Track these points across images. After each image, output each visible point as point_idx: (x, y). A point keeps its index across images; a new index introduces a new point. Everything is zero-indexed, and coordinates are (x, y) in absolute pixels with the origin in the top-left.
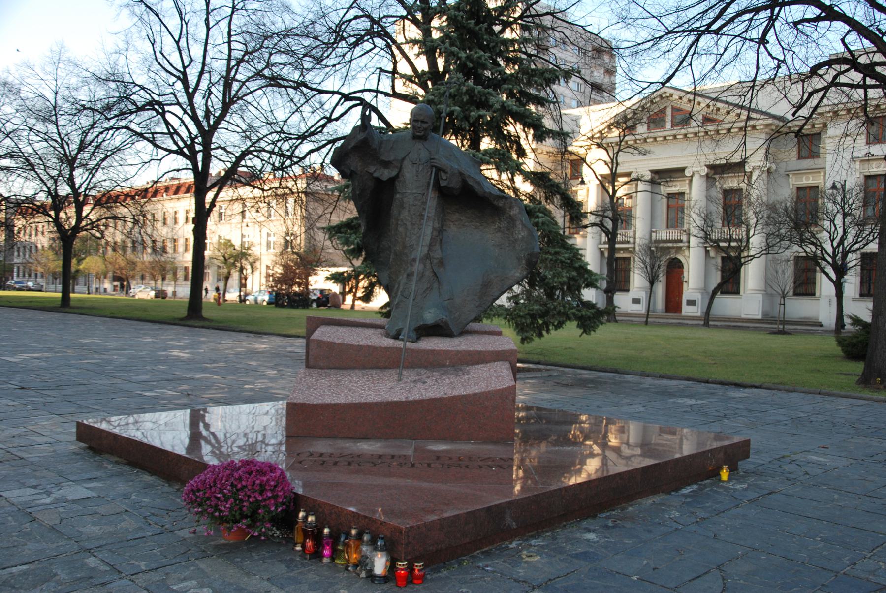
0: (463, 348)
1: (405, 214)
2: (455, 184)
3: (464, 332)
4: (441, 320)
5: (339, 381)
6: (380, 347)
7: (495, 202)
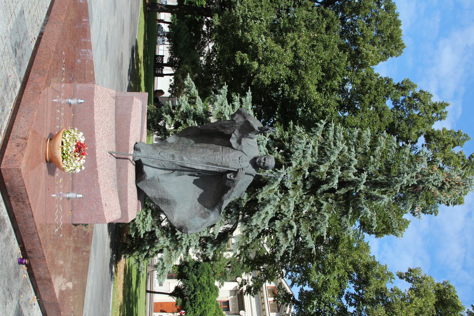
0: (129, 190)
1: (210, 152)
5: (108, 115)
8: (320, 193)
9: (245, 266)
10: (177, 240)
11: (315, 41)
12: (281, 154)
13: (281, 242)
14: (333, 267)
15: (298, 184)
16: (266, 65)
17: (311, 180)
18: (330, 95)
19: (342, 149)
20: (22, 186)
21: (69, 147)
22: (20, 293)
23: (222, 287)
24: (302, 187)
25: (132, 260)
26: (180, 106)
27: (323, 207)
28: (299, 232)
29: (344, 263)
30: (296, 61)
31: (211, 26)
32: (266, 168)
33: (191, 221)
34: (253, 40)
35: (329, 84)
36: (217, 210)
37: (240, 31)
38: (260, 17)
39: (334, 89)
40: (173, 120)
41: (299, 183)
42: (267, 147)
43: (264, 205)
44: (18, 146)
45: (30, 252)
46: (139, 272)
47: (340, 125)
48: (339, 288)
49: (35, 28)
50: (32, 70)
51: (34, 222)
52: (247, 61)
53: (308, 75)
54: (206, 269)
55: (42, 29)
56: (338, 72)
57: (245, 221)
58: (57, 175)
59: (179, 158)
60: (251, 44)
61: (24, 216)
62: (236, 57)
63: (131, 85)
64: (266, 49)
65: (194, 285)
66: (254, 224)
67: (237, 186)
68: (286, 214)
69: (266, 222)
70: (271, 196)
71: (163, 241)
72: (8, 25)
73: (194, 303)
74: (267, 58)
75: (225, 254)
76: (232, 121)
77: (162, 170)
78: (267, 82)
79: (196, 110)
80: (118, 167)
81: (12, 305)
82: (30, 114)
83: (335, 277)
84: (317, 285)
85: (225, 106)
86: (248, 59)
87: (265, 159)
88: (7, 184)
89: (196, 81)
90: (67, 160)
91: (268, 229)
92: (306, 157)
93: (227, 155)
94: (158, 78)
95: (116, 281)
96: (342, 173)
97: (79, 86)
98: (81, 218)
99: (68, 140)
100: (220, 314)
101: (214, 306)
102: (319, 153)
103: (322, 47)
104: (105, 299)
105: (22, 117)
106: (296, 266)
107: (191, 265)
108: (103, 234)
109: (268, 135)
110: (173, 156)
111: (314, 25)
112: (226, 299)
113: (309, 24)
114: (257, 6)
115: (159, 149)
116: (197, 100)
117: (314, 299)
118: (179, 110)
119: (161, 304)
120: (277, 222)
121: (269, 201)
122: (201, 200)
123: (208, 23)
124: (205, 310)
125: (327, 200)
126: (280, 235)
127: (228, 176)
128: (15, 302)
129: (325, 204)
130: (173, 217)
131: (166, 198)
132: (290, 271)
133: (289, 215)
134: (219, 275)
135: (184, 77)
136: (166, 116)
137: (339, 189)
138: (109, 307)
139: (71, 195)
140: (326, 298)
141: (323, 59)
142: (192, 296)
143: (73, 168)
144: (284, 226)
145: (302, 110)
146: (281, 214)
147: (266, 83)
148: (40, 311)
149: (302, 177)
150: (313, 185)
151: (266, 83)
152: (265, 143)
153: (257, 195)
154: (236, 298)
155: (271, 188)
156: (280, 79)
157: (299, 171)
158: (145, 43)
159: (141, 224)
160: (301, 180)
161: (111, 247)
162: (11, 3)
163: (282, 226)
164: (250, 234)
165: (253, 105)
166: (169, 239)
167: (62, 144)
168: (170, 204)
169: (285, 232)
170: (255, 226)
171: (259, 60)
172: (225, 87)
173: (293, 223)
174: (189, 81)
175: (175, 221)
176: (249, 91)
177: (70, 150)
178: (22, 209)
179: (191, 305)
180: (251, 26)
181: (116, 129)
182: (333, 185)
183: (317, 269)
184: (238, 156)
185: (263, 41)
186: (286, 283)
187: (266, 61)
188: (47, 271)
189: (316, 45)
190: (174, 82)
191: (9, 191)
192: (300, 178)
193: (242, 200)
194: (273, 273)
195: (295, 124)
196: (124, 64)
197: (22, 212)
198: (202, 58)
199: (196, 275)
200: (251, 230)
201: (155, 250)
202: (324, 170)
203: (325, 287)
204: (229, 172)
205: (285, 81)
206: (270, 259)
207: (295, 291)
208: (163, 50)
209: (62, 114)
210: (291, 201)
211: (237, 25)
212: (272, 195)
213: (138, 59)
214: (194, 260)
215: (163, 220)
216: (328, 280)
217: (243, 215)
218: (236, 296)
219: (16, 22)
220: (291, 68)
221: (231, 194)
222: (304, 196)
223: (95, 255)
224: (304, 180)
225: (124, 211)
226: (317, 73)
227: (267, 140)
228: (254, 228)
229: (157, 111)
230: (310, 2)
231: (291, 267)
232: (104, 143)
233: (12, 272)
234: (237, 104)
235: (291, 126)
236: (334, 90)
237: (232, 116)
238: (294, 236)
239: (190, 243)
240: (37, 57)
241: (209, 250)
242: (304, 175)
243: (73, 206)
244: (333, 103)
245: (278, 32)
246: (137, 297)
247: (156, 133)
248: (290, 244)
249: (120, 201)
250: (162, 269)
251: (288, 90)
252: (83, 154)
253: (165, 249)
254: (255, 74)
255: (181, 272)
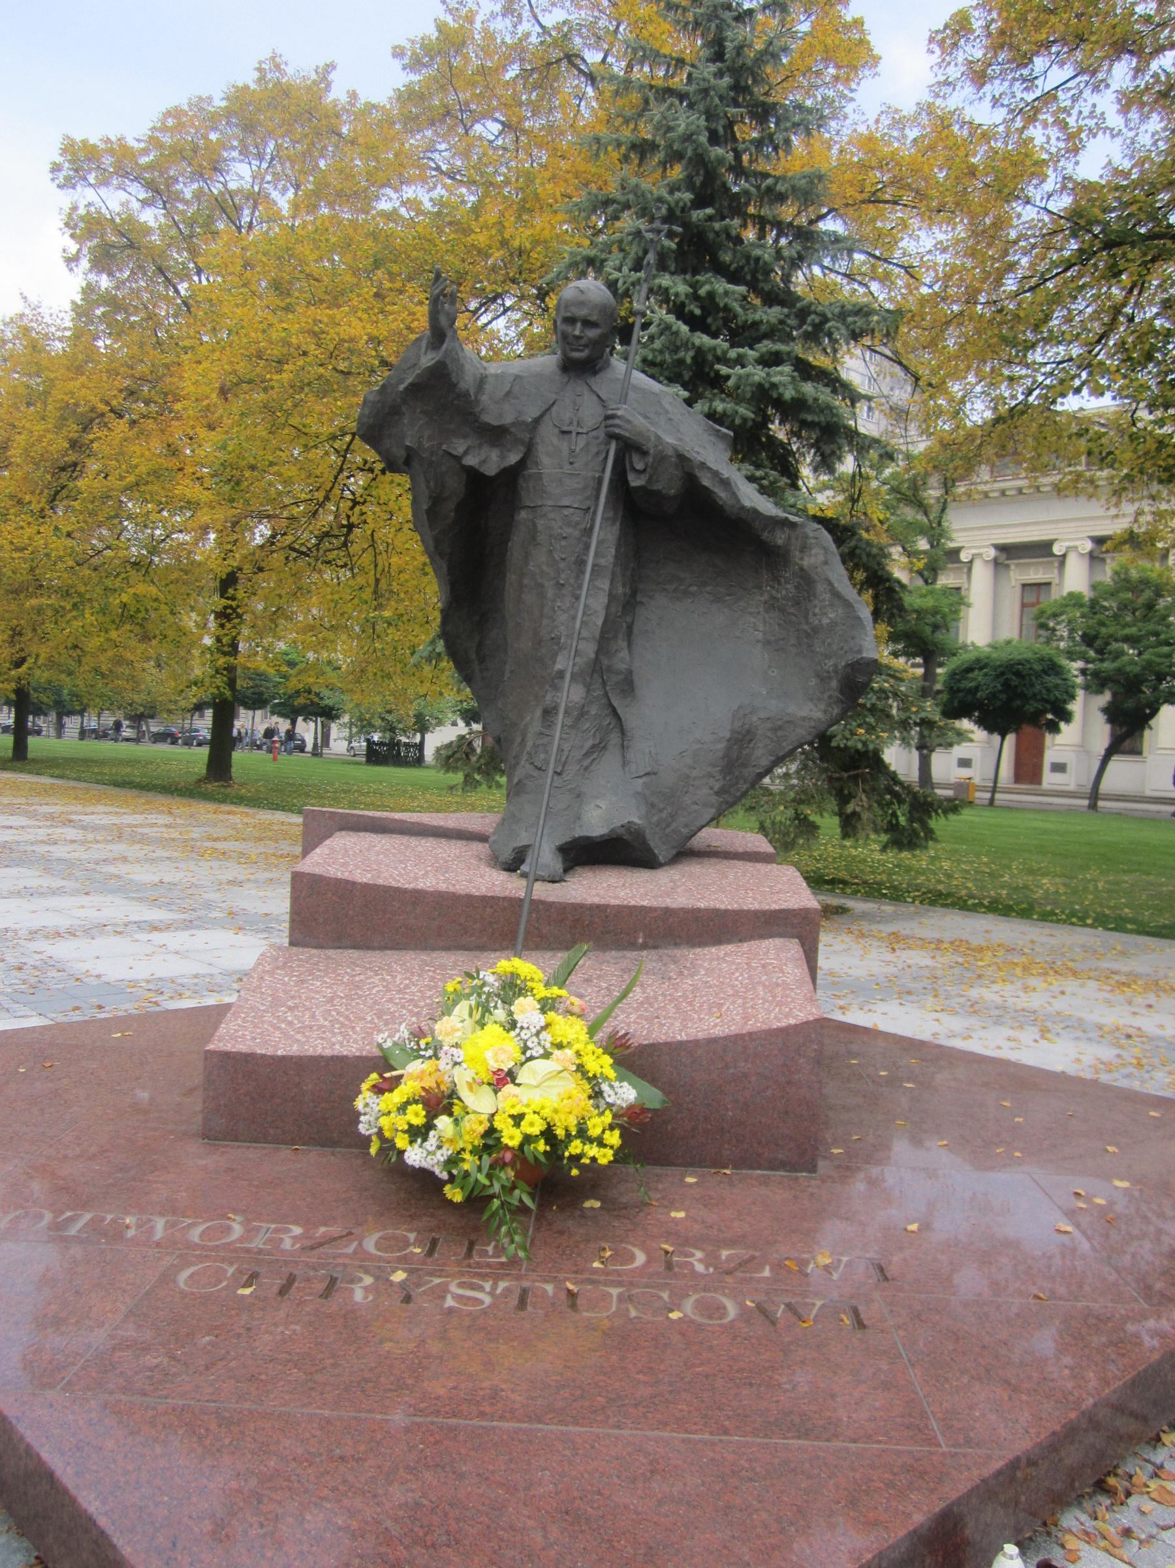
1: (539, 560)
2: (668, 484)
3: (685, 853)
4: (628, 827)
6: (469, 897)
7: (765, 536)
130: (803, 719)
131: (721, 746)
168: (748, 732)
184: (555, 441)
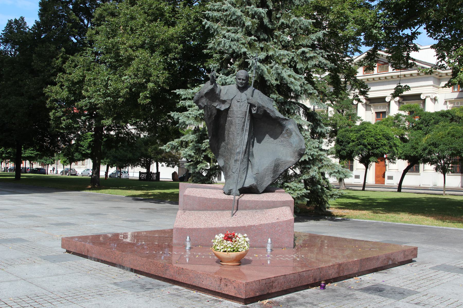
0: (265, 199)
1: (233, 129)
5: (200, 217)
8: (272, 25)
9: (340, 96)
10: (313, 159)
11: (127, 28)
12: (234, 61)
13: (317, 63)
14: (342, 13)
15: (263, 46)
16: (150, 75)
17: (259, 33)
18: (179, 13)
19: (230, 3)
20: (260, 282)
21: (228, 246)
22: (350, 288)
23: (362, 118)
24: (266, 43)
25: (331, 201)
26: (190, 156)
27: (285, 22)
28: (308, 45)
29: (338, 3)
30: (146, 46)
31: (112, 127)
32: (247, 78)
33: (294, 146)
34: (127, 88)
35: (168, 15)
36: (284, 123)
37: (119, 99)
38: (105, 81)
39: (172, 9)
40: (202, 162)
41: (262, 45)
42: (227, 74)
43: (282, 79)
44: (227, 285)
45: (315, 280)
46: (342, 196)
47: (207, 6)
48: (362, 9)
49: (127, 275)
50: (164, 276)
51: (290, 274)
52: (147, 93)
53: (160, 35)
54: (344, 133)
55: (127, 270)
56: (157, 6)
57: (297, 96)
58: (251, 258)
59: (238, 156)
60: (131, 90)
61: (285, 282)
62: (143, 104)
63: (169, 202)
64: (136, 75)
65: (359, 145)
66: (299, 88)
67: (263, 104)
68: (291, 58)
69: (298, 76)
70: (274, 72)
71: (314, 172)
72: (127, 294)
73: (375, 145)
74: (144, 75)
75: (330, 115)
76: (205, 108)
77: (249, 171)
78: (166, 74)
79: (193, 141)
80: (245, 209)
81: (359, 294)
82: (201, 277)
83: (352, 12)
84: (358, 30)
85: (190, 114)
86: (145, 92)
87: (240, 79)
88: (258, 294)
89: (165, 142)
90: (239, 248)
91: (305, 74)
92: (238, 38)
93: (235, 113)
94: (160, 177)
95: (350, 217)
96: (253, 4)
97: (175, 241)
98: (289, 240)
99: (222, 247)
100: (387, 121)
101: (379, 126)
102: (233, 26)
103: (133, 22)
104: (365, 226)
105: (203, 283)
106: (342, 47)
107: (339, 148)
108: (306, 226)
109: (217, 74)
110: (236, 161)
111: (112, 30)
112: (374, 114)
113: (111, 34)
114: (95, 84)
115: (230, 173)
116: (184, 140)
117: (372, 32)
118: (193, 157)
119: (377, 177)
120: (298, 66)
121: (279, 74)
122: (275, 136)
123: (109, 130)
124: (383, 135)
125: (279, 18)
126: (311, 63)
127: (254, 112)
128: (356, 292)
129: (282, 20)
132: (346, 53)
133: (292, 55)
134: (350, 121)
135: (162, 151)
136: (198, 169)
137: (268, 7)
138: (374, 223)
139: (269, 248)
140: (371, 20)
141: (144, 20)
142: (369, 147)
143: (246, 243)
144: (302, 60)
145: (193, 41)
146: (291, 62)
147: (167, 75)
148: (367, 275)
149: (256, 43)
150: (264, 31)
151: (167, 75)
152: (224, 77)
153: (272, 85)
154: (373, 105)
155: (266, 72)
156: (164, 62)
157: (251, 45)
158: (129, 189)
159: (297, 192)
160: (259, 43)
161: (319, 220)
162: (109, 292)
163: (302, 61)
164: (309, 92)
165: (189, 88)
166: (312, 166)
167: (225, 251)
169: (307, 60)
170: (301, 87)
171: (146, 82)
172: (172, 114)
173: (300, 51)
174: (166, 148)
175: (292, 159)
176: (175, 91)
177: (231, 245)
178: (278, 284)
179: (377, 148)
180: (114, 89)
181: (212, 210)
182: (264, 13)
183: (342, 29)
185: (128, 78)
186: (357, 57)
187: (147, 75)
188: (332, 267)
189: (131, 27)
190: (164, 162)
191: (263, 293)
192: (257, 44)
193: (277, 98)
194: (347, 70)
195: (206, 48)
196: (150, 207)
197: (281, 284)
198: (142, 136)
199: (349, 143)
200: (306, 90)
201: (322, 181)
202: (250, 22)
203: (360, 22)
204: (250, 111)
205: (166, 57)
206: (334, 72)
207: (365, 49)
208: (134, 172)
209: (199, 254)
210: (279, 53)
211: (112, 103)
212: (273, 71)
213: (144, 195)
214: (335, 145)
215: (294, 172)
216: (354, 18)
217: (292, 97)
218: (372, 105)
219: (124, 288)
220: (153, 51)
221: (271, 110)
222: (275, 40)
223: (325, 233)
224: (260, 40)
225: (284, 204)
226: (157, 26)
227: (221, 75)
228: (303, 88)
229: (194, 176)
230: (88, 32)
231: (342, 53)
232: (225, 220)
233: (331, 294)
234: (188, 103)
235: (208, 51)
236: (173, 10)
237: (200, 108)
238: (311, 51)
239: (316, 148)
240: (152, 272)
241: (323, 130)
242: (255, 40)
243: (278, 247)
244: (187, 10)
245: (119, 63)
246: (368, 199)
247: (214, 178)
248: (319, 54)
249: (275, 208)
250: (340, 173)
251: (174, 54)
252: (234, 235)
253: (321, 170)
254: (159, 86)
255: (346, 156)
